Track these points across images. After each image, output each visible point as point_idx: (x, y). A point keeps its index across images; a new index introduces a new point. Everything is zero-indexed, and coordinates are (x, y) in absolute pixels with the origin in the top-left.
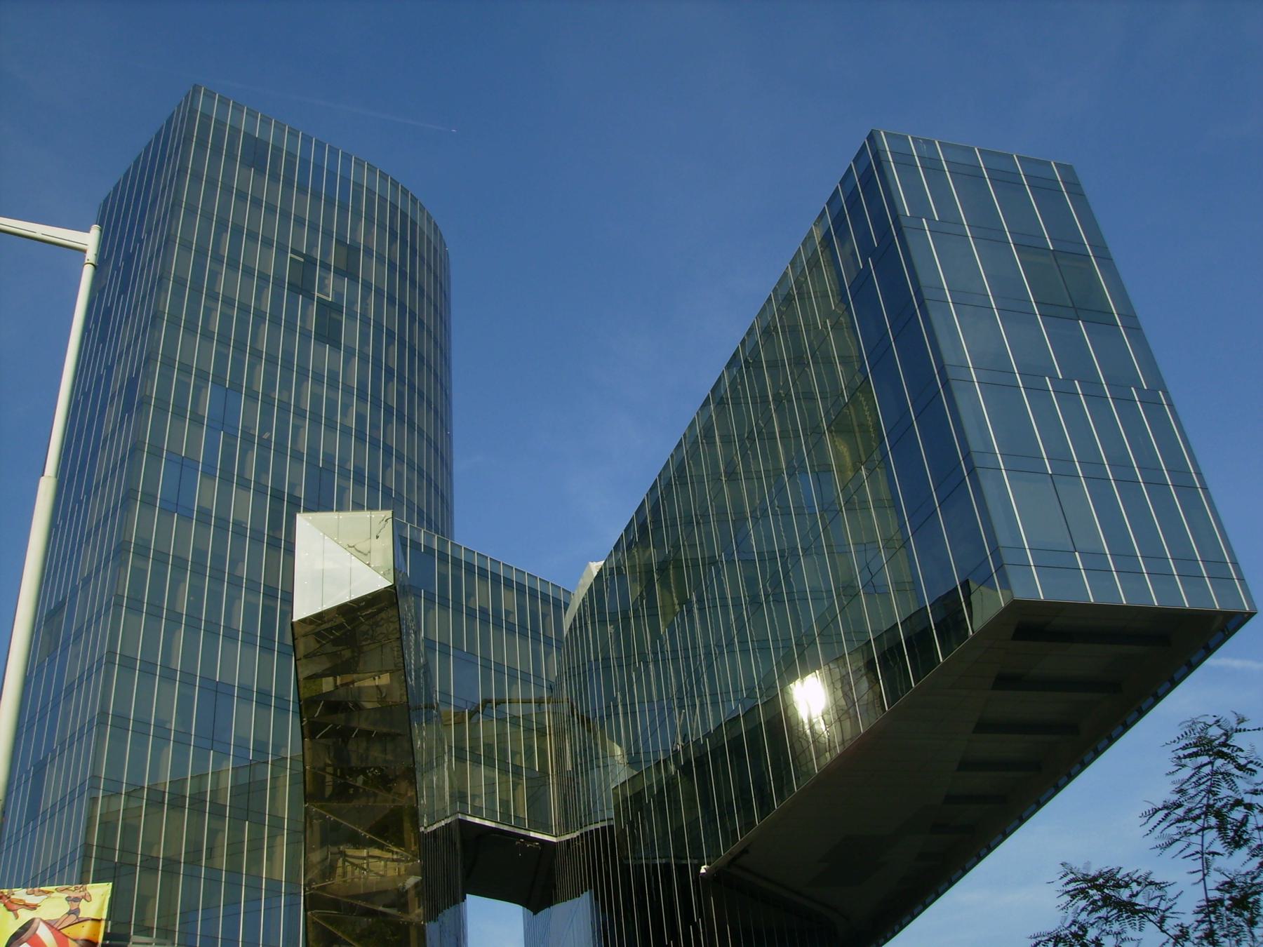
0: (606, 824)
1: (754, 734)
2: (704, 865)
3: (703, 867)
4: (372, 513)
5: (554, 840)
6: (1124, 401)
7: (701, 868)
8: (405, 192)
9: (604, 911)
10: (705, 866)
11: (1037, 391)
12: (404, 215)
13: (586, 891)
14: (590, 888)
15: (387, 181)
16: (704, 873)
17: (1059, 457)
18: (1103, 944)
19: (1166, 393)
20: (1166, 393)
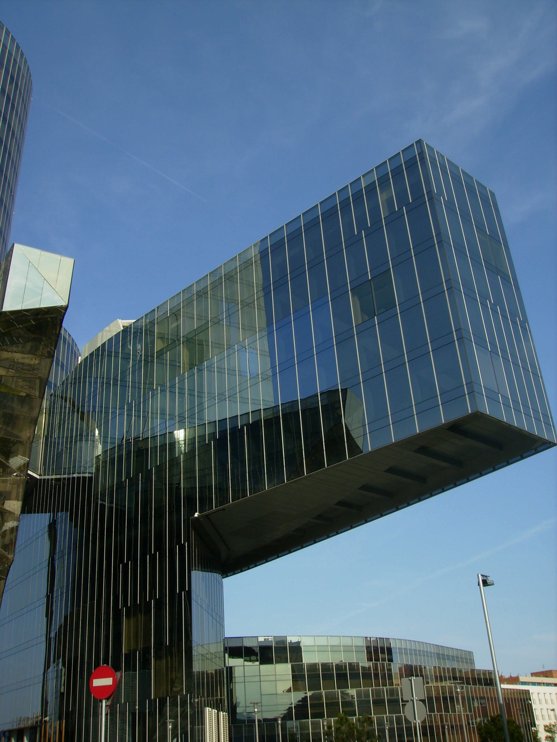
0: (87, 475)
1: (163, 446)
2: (197, 512)
3: (196, 513)
4: (42, 251)
5: (38, 477)
6: (514, 323)
7: (195, 514)
8: (13, 40)
9: (76, 526)
10: (197, 513)
11: (484, 305)
12: (10, 54)
13: (46, 512)
14: (67, 510)
15: (3, 29)
16: (197, 517)
17: (493, 344)
18: (291, 641)
19: (528, 324)
20: (528, 324)
